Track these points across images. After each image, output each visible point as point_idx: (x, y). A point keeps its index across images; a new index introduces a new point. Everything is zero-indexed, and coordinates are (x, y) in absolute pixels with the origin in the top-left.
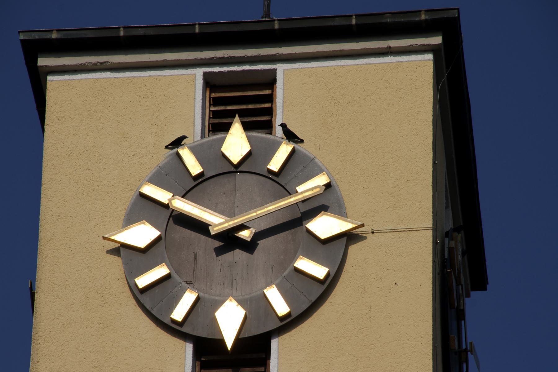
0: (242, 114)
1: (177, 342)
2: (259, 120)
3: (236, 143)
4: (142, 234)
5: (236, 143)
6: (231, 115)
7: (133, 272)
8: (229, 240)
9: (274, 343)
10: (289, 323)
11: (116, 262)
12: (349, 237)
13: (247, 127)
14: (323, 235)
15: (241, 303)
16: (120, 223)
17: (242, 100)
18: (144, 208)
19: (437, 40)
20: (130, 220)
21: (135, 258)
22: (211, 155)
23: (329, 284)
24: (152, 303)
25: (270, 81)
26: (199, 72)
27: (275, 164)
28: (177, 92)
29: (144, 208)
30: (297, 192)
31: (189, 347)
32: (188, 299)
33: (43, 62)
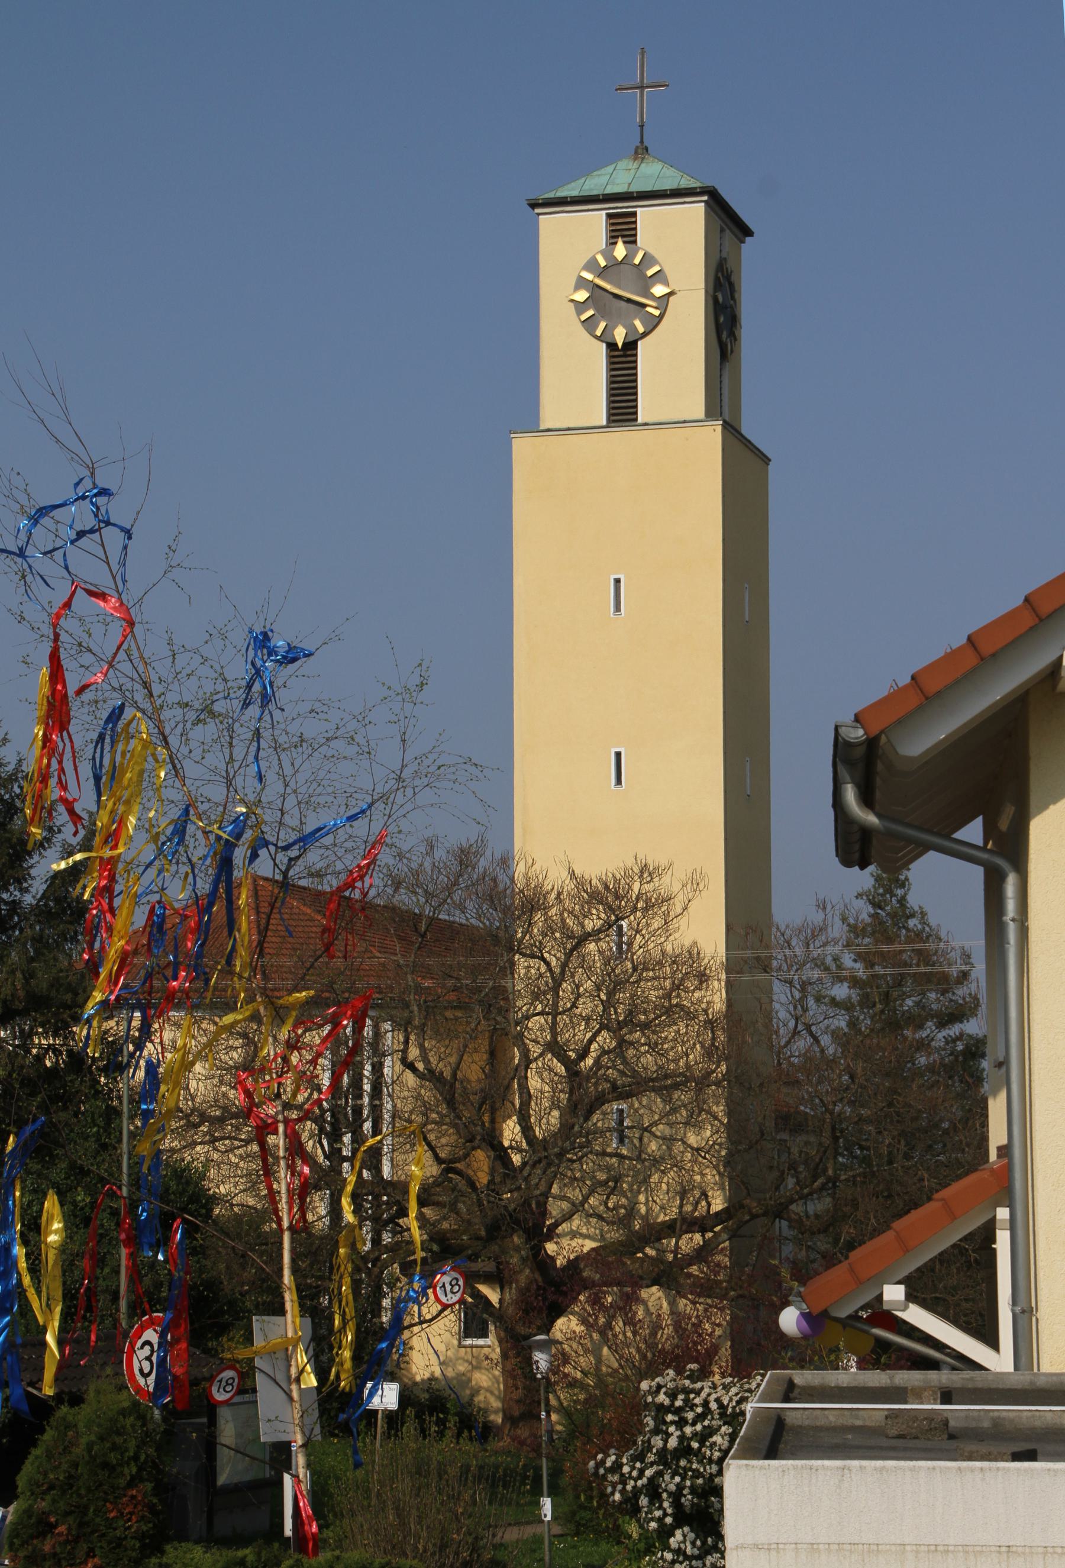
0: (623, 236)
1: (599, 343)
2: (631, 240)
3: (620, 251)
4: (582, 296)
6: (617, 237)
7: (579, 312)
9: (639, 343)
10: (644, 335)
11: (572, 305)
12: (671, 294)
13: (625, 242)
14: (658, 295)
15: (625, 327)
16: (764, 1452)
17: (623, 228)
18: (581, 283)
19: (705, 198)
20: (577, 288)
21: (580, 307)
22: (608, 254)
23: (661, 316)
24: (589, 325)
25: (634, 214)
26: (604, 213)
27: (637, 261)
28: (596, 220)
29: (581, 283)
30: (349, 1394)
31: (604, 345)
32: (603, 325)
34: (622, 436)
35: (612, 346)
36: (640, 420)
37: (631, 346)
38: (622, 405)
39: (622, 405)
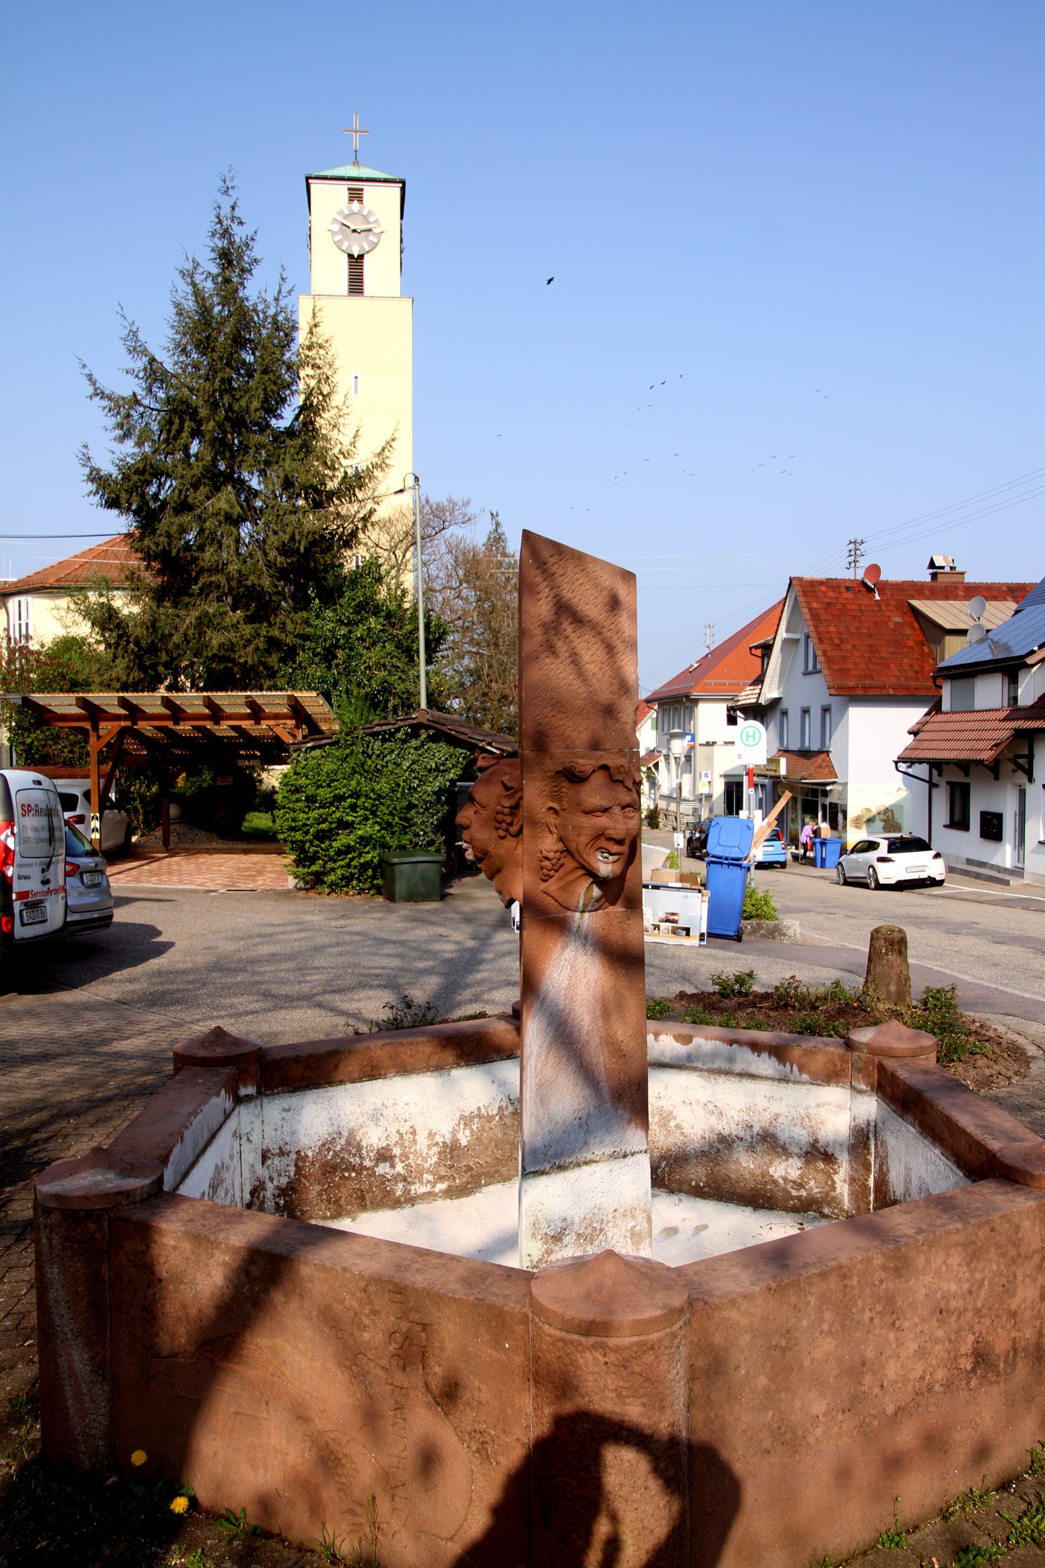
5: (355, 206)
8: (354, 231)
20: (332, 223)
21: (334, 234)
24: (338, 244)
29: (335, 220)
33: (310, 181)
34: (356, 300)
35: (351, 256)
36: (366, 293)
37: (361, 257)
38: (356, 285)
39: (356, 285)
